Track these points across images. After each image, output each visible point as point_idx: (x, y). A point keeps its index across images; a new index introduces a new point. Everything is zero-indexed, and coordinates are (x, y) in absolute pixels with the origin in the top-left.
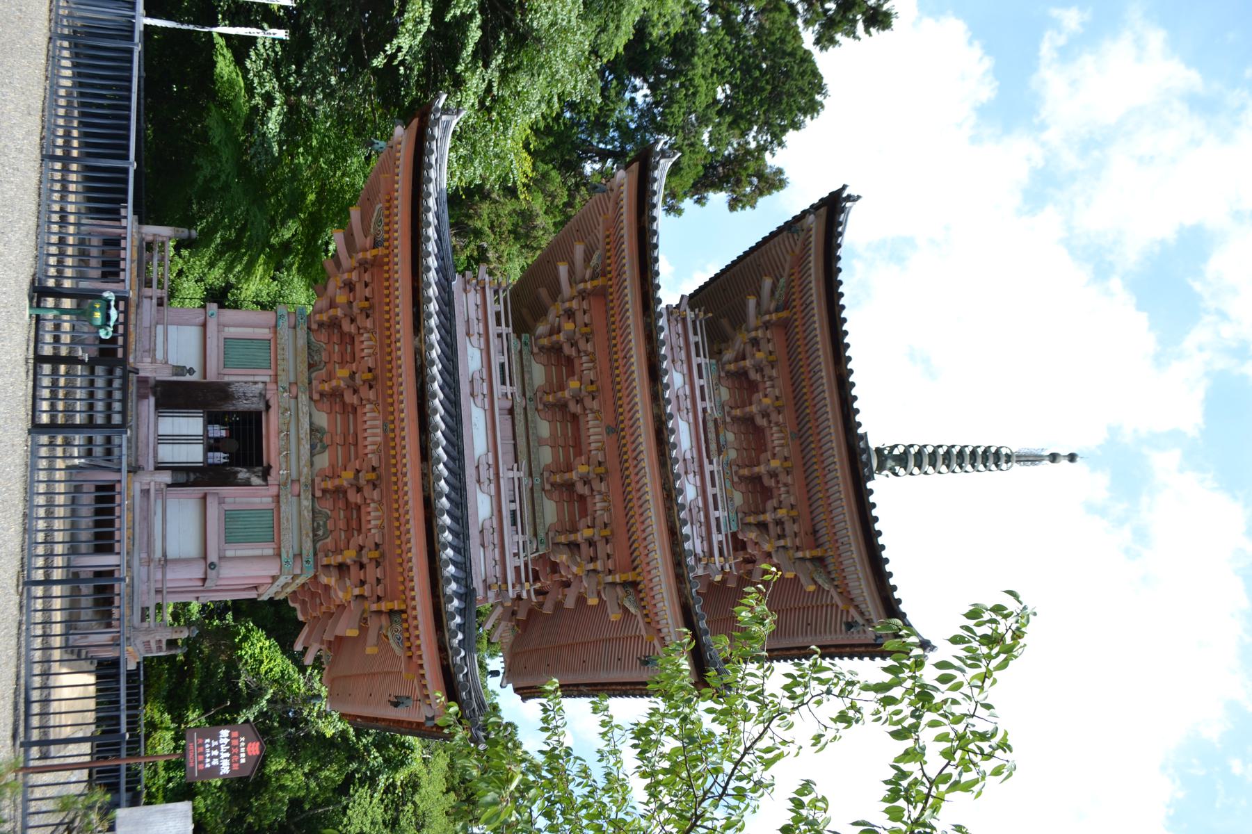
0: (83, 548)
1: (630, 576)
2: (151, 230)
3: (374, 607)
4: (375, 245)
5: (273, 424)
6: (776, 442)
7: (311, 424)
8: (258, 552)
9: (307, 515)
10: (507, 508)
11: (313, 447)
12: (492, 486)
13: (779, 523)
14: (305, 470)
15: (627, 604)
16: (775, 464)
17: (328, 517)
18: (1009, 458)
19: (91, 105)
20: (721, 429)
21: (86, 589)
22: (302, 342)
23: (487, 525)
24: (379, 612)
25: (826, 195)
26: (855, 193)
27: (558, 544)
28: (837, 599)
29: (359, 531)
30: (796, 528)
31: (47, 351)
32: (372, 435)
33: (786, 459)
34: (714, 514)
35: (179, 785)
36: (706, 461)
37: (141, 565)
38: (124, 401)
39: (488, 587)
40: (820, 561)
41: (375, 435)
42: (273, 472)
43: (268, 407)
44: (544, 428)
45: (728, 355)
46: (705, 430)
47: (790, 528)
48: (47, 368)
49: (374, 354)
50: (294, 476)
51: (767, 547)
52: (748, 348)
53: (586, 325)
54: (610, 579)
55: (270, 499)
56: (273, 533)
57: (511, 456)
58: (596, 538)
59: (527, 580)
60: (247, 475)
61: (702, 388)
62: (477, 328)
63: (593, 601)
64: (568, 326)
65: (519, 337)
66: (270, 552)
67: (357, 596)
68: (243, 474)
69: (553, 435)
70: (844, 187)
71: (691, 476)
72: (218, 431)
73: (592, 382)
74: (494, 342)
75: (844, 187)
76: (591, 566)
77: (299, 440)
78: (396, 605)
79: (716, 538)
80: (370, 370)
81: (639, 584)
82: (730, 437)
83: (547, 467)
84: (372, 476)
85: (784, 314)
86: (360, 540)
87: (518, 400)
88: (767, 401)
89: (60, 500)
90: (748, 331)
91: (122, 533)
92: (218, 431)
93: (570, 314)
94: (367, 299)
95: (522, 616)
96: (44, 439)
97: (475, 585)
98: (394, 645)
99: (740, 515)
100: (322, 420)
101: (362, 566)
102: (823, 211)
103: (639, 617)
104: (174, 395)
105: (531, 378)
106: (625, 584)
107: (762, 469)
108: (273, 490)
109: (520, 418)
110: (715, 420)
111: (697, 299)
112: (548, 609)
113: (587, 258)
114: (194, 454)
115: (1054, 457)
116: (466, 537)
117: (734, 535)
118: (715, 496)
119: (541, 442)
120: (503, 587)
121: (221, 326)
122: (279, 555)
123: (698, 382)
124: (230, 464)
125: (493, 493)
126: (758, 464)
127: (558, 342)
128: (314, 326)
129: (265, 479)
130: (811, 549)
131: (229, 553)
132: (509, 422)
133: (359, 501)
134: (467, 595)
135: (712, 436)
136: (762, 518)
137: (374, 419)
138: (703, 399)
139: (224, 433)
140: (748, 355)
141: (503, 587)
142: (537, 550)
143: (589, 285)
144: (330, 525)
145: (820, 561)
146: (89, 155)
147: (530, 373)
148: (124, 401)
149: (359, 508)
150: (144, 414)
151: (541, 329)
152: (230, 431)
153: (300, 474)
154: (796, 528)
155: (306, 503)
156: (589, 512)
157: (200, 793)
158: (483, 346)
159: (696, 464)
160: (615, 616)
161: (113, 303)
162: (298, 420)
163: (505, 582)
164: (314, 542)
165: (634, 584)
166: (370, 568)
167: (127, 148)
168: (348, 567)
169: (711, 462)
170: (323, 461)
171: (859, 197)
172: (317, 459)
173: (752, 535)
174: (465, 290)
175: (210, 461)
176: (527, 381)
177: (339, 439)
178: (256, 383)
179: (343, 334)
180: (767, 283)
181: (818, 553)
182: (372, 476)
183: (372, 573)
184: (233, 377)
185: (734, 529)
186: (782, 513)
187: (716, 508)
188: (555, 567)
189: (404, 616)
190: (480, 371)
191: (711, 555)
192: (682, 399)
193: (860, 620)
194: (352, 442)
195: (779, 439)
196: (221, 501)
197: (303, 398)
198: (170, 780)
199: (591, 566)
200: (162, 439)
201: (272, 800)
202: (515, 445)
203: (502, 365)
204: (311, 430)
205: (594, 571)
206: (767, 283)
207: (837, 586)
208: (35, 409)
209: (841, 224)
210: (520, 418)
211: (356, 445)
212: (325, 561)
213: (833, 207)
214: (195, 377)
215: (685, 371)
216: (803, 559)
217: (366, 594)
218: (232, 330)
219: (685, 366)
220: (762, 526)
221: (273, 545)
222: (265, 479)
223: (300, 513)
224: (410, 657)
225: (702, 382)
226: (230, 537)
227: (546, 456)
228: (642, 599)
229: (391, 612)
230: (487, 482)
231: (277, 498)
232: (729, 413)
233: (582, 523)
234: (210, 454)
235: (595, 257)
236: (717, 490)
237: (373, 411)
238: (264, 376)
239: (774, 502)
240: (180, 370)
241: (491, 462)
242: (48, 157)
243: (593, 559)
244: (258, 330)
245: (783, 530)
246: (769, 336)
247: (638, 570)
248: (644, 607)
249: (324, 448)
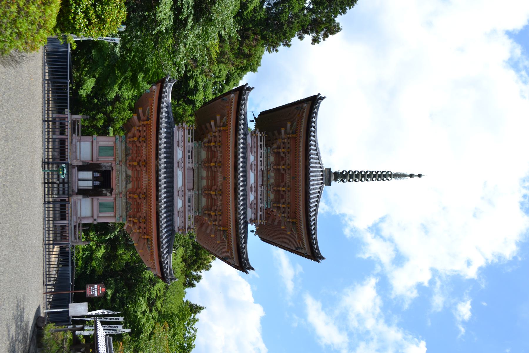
0: (57, 219)
2: (75, 117)
5: (114, 174)
7: (126, 174)
8: (109, 215)
9: (124, 204)
11: (126, 182)
14: (124, 190)
17: (131, 204)
18: (391, 176)
19: (56, 83)
21: (58, 205)
22: (124, 148)
23: (181, 210)
30: (289, 210)
35: (87, 256)
39: (179, 230)
41: (145, 181)
42: (114, 191)
43: (113, 170)
44: (204, 173)
47: (287, 210)
50: (120, 191)
52: (282, 145)
56: (114, 210)
62: (181, 144)
69: (207, 176)
71: (253, 193)
72: (97, 175)
76: (214, 223)
77: (122, 180)
82: (272, 174)
83: (204, 188)
85: (294, 136)
89: (51, 212)
91: (69, 215)
92: (97, 175)
96: (47, 206)
100: (130, 173)
102: (310, 102)
104: (84, 167)
108: (114, 196)
109: (196, 171)
113: (221, 121)
114: (89, 184)
115: (411, 176)
119: (202, 178)
121: (97, 142)
122: (115, 216)
129: (111, 194)
130: (293, 219)
131: (100, 215)
134: (171, 233)
139: (99, 175)
144: (131, 207)
146: (54, 78)
147: (201, 155)
150: (74, 173)
152: (101, 174)
153: (122, 191)
154: (289, 210)
155: (124, 201)
157: (94, 260)
162: (122, 174)
163: (185, 228)
164: (126, 212)
167: (67, 75)
170: (130, 186)
171: (325, 98)
172: (128, 186)
177: (135, 179)
180: (289, 125)
184: (102, 159)
193: (302, 247)
194: (138, 179)
196: (98, 200)
197: (124, 166)
198: (84, 254)
200: (80, 179)
201: (119, 263)
204: (126, 176)
206: (289, 125)
210: (196, 171)
212: (129, 219)
218: (101, 143)
220: (279, 208)
222: (111, 194)
223: (122, 203)
226: (100, 211)
227: (204, 183)
235: (224, 119)
238: (111, 159)
242: (44, 121)
244: (110, 143)
249: (130, 182)
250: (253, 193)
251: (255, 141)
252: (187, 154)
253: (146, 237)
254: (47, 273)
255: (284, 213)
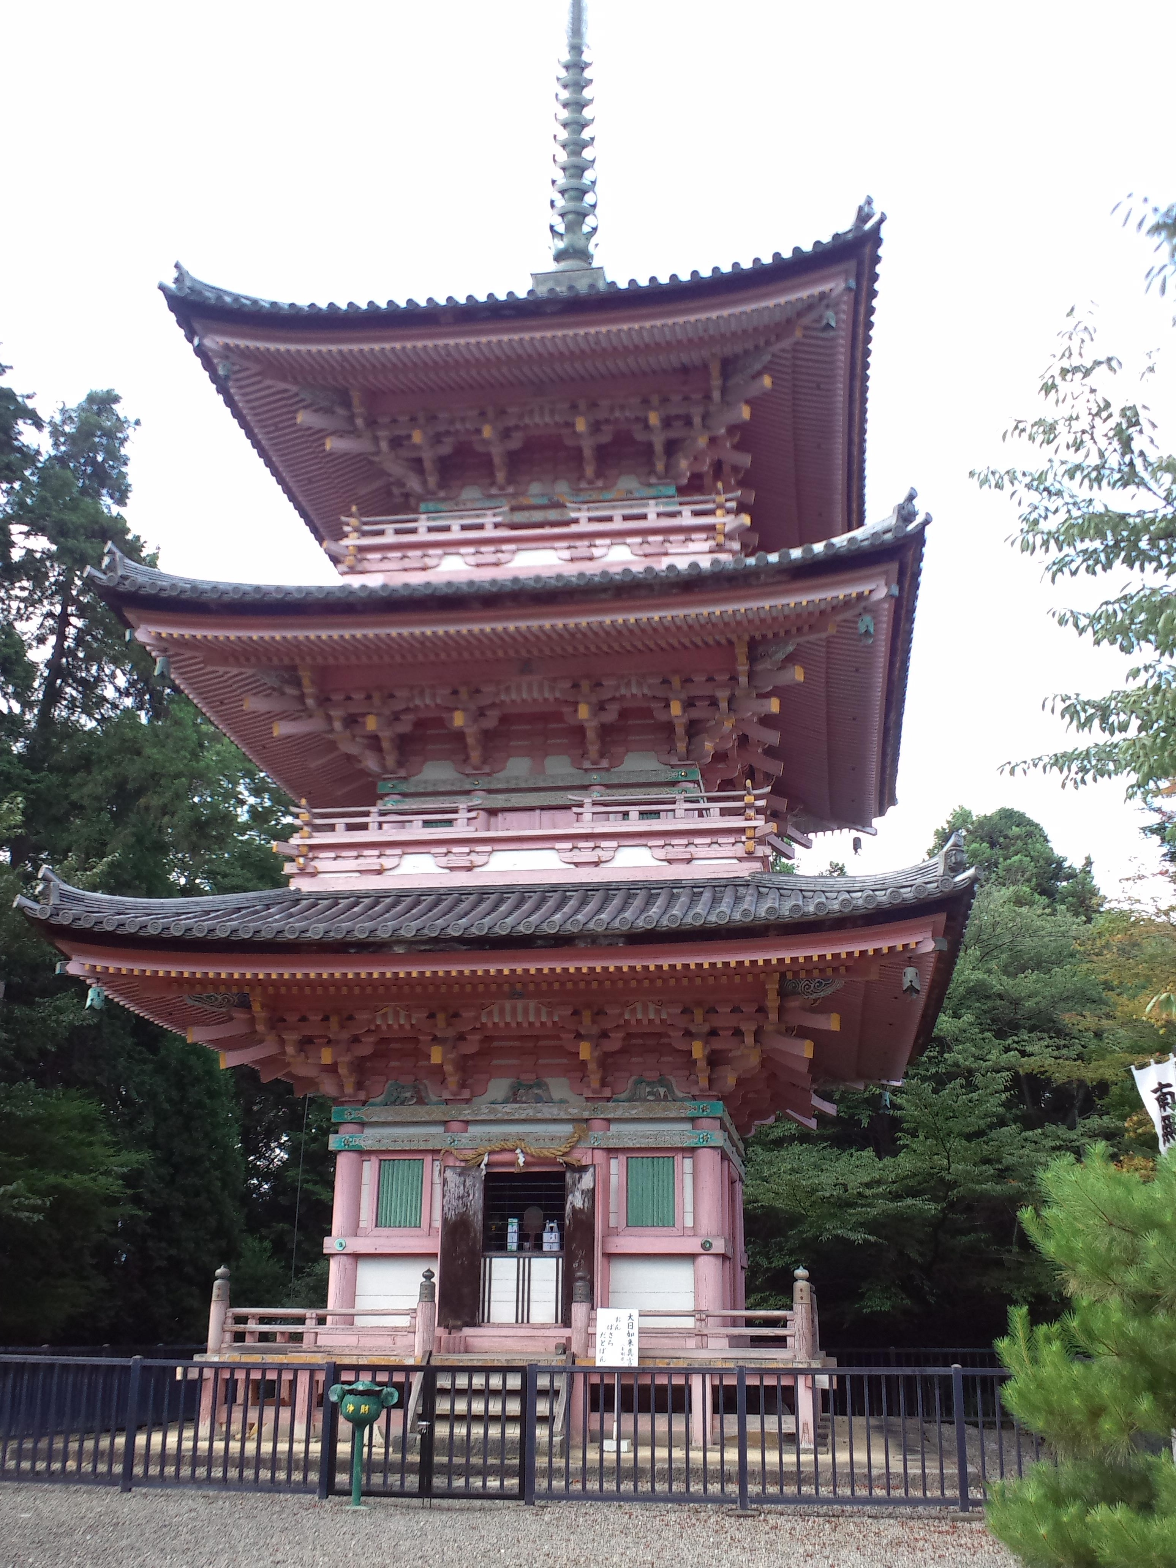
1: (741, 652)
3: (773, 1016)
4: (245, 1004)
6: (547, 419)
7: (506, 1101)
10: (635, 825)
12: (604, 844)
13: (667, 423)
15: (781, 656)
16: (581, 425)
20: (525, 501)
24: (781, 1010)
25: (172, 317)
26: (175, 274)
27: (688, 751)
28: (786, 344)
29: (660, 1035)
30: (676, 398)
31: (413, 1481)
32: (528, 1014)
33: (483, 414)
34: (652, 521)
36: (574, 529)
37: (704, 1347)
38: (471, 1370)
40: (728, 366)
41: (526, 1011)
45: (414, 484)
46: (525, 530)
48: (439, 1482)
49: (408, 1008)
51: (702, 442)
53: (369, 697)
54: (743, 680)
55: (614, 1163)
57: (559, 815)
58: (683, 696)
59: (740, 798)
60: (578, 1194)
61: (464, 528)
62: (370, 859)
63: (774, 705)
64: (371, 724)
65: (381, 797)
66: (688, 1163)
67: (756, 1041)
68: (576, 1200)
70: (162, 288)
73: (455, 692)
74: (390, 833)
75: (162, 288)
76: (724, 705)
78: (772, 987)
79: (687, 519)
80: (432, 1016)
81: (753, 638)
82: (535, 488)
84: (441, 1018)
86: (676, 1034)
87: (476, 802)
88: (487, 432)
90: (377, 453)
93: (352, 721)
94: (326, 1019)
95: (782, 804)
96: (541, 1484)
97: (745, 874)
98: (829, 991)
99: (583, 485)
101: (713, 1033)
103: (801, 640)
104: (459, 1299)
105: (444, 782)
106: (753, 659)
107: (497, 452)
109: (499, 801)
110: (513, 509)
111: (324, 527)
112: (777, 768)
114: (545, 1272)
116: (676, 884)
117: (682, 491)
118: (626, 518)
120: (749, 833)
123: (456, 534)
124: (561, 1218)
125: (614, 844)
126: (579, 450)
127: (392, 740)
128: (362, 1096)
132: (510, 816)
133: (477, 1037)
135: (537, 516)
136: (659, 448)
137: (502, 1011)
138: (481, 527)
140: (414, 455)
141: (749, 833)
142: (697, 782)
143: (309, 690)
145: (728, 366)
148: (471, 1370)
149: (488, 1039)
151: (371, 763)
154: (676, 398)
156: (645, 705)
158: (398, 851)
159: (578, 543)
160: (798, 674)
161: (347, 1387)
163: (742, 830)
165: (753, 644)
166: (718, 1022)
168: (713, 1052)
169: (576, 521)
173: (683, 464)
174: (314, 875)
175: (556, 1248)
176: (449, 788)
178: (445, 1182)
179: (375, 1056)
181: (715, 370)
182: (441, 1018)
183: (724, 1019)
185: (672, 491)
186: (654, 419)
187: (644, 517)
188: (720, 757)
189: (789, 975)
190: (435, 855)
191: (711, 528)
192: (648, 549)
195: (542, 414)
199: (724, 705)
200: (523, 1317)
202: (543, 808)
203: (427, 824)
205: (730, 702)
207: (768, 343)
208: (502, 1495)
209: (219, 298)
210: (499, 801)
211: (537, 1038)
213: (196, 309)
214: (436, 1270)
215: (439, 551)
216: (724, 391)
217: (754, 1028)
219: (431, 552)
221: (678, 1157)
224: (847, 969)
225: (455, 527)
228: (775, 635)
229: (782, 994)
230: (598, 852)
231: (612, 1151)
232: (502, 488)
233: (661, 717)
234: (546, 1248)
236: (617, 514)
237: (490, 1014)
239: (637, 428)
240: (427, 1291)
241: (569, 845)
243: (714, 703)
245: (678, 417)
246: (386, 420)
247: (734, 638)
248: (787, 632)
250: (596, 552)
251: (378, 556)
252: (416, 831)
253: (772, 1001)
254: (899, 1493)
255: (688, 422)
